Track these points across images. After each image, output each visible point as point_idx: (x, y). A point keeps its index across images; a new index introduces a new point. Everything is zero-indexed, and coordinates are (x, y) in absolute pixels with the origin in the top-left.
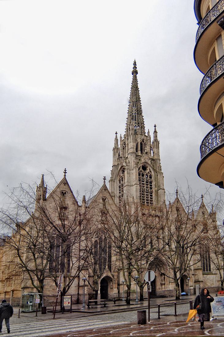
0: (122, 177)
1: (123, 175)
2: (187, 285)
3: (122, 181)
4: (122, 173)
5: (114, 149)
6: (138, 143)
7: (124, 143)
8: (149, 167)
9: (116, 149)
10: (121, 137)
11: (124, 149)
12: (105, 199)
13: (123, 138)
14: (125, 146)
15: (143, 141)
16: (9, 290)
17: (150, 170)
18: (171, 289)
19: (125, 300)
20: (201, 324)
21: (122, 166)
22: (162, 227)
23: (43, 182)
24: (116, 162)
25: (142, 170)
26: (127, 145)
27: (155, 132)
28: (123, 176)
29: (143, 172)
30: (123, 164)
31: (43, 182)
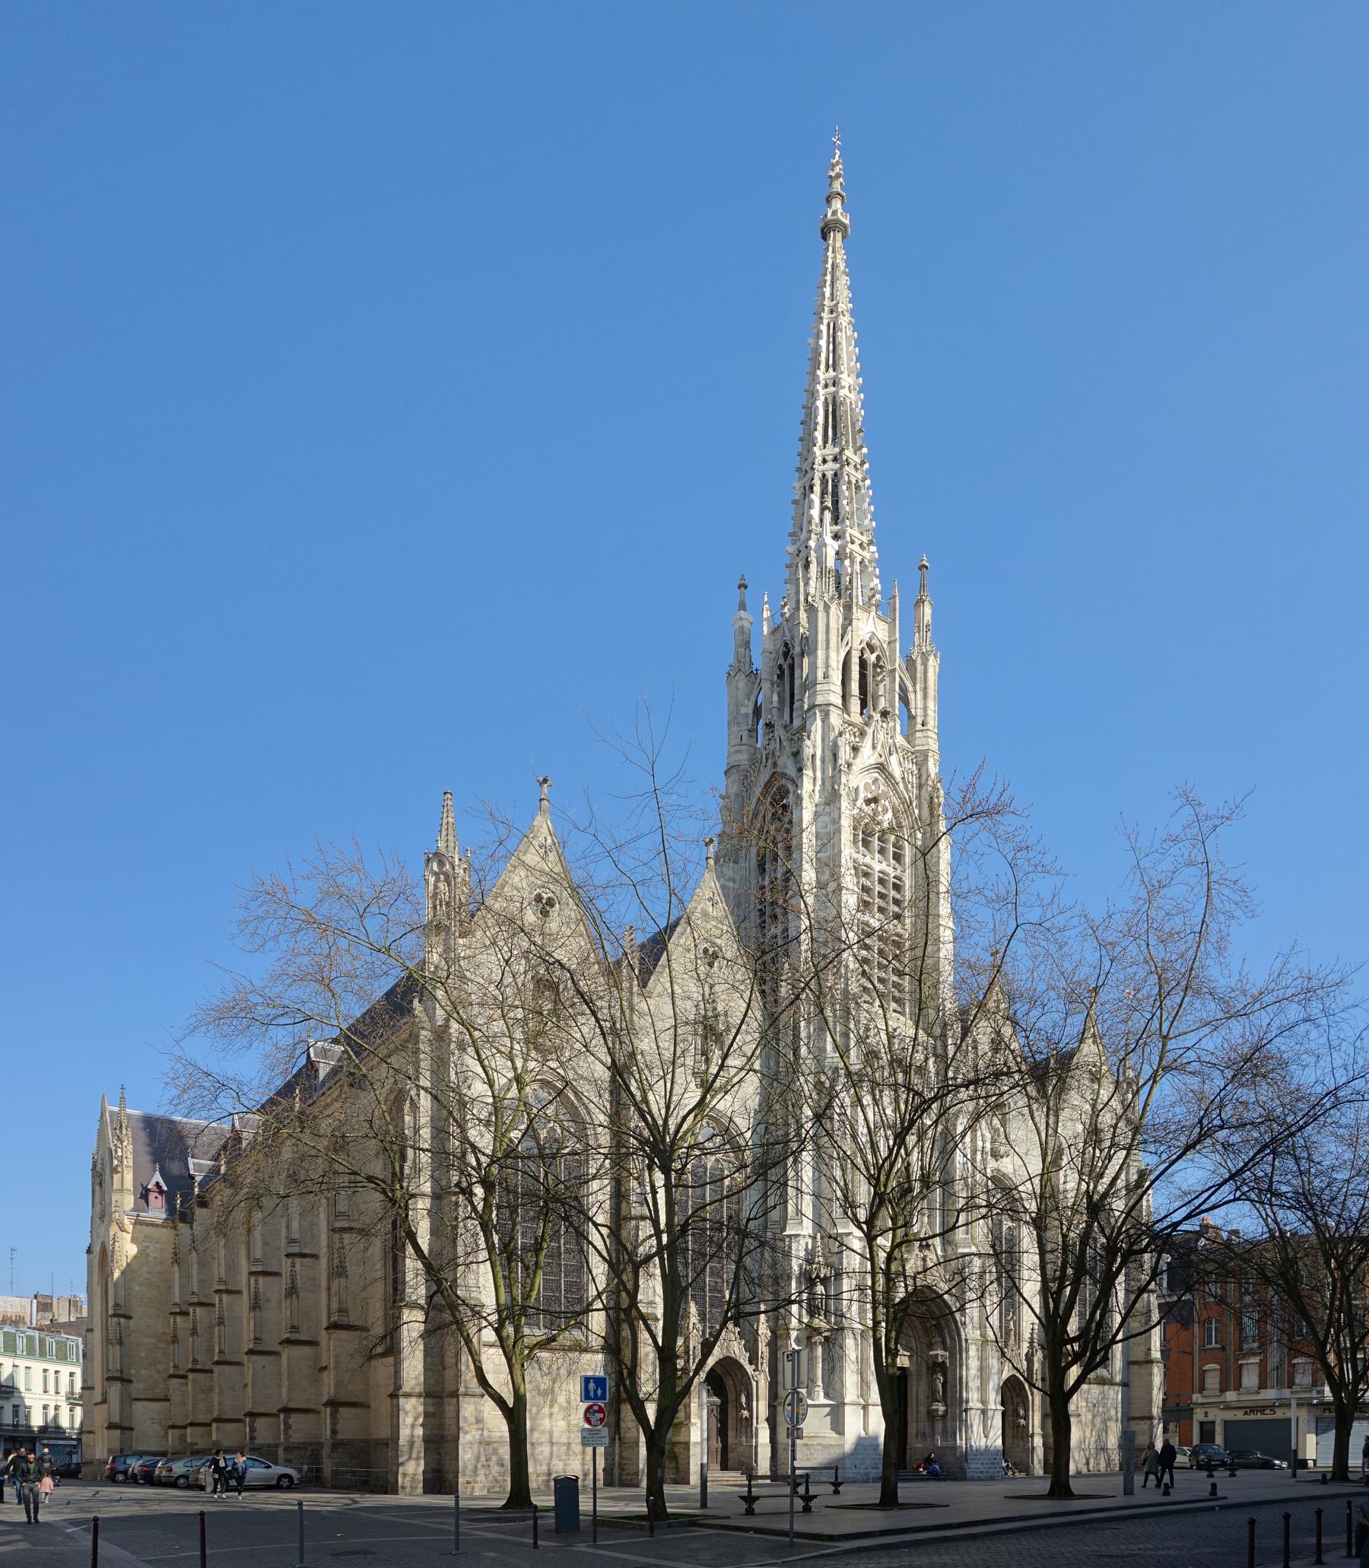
2: (121, 1343)
6: (848, 654)
7: (782, 649)
11: (781, 676)
14: (785, 667)
24: (744, 748)
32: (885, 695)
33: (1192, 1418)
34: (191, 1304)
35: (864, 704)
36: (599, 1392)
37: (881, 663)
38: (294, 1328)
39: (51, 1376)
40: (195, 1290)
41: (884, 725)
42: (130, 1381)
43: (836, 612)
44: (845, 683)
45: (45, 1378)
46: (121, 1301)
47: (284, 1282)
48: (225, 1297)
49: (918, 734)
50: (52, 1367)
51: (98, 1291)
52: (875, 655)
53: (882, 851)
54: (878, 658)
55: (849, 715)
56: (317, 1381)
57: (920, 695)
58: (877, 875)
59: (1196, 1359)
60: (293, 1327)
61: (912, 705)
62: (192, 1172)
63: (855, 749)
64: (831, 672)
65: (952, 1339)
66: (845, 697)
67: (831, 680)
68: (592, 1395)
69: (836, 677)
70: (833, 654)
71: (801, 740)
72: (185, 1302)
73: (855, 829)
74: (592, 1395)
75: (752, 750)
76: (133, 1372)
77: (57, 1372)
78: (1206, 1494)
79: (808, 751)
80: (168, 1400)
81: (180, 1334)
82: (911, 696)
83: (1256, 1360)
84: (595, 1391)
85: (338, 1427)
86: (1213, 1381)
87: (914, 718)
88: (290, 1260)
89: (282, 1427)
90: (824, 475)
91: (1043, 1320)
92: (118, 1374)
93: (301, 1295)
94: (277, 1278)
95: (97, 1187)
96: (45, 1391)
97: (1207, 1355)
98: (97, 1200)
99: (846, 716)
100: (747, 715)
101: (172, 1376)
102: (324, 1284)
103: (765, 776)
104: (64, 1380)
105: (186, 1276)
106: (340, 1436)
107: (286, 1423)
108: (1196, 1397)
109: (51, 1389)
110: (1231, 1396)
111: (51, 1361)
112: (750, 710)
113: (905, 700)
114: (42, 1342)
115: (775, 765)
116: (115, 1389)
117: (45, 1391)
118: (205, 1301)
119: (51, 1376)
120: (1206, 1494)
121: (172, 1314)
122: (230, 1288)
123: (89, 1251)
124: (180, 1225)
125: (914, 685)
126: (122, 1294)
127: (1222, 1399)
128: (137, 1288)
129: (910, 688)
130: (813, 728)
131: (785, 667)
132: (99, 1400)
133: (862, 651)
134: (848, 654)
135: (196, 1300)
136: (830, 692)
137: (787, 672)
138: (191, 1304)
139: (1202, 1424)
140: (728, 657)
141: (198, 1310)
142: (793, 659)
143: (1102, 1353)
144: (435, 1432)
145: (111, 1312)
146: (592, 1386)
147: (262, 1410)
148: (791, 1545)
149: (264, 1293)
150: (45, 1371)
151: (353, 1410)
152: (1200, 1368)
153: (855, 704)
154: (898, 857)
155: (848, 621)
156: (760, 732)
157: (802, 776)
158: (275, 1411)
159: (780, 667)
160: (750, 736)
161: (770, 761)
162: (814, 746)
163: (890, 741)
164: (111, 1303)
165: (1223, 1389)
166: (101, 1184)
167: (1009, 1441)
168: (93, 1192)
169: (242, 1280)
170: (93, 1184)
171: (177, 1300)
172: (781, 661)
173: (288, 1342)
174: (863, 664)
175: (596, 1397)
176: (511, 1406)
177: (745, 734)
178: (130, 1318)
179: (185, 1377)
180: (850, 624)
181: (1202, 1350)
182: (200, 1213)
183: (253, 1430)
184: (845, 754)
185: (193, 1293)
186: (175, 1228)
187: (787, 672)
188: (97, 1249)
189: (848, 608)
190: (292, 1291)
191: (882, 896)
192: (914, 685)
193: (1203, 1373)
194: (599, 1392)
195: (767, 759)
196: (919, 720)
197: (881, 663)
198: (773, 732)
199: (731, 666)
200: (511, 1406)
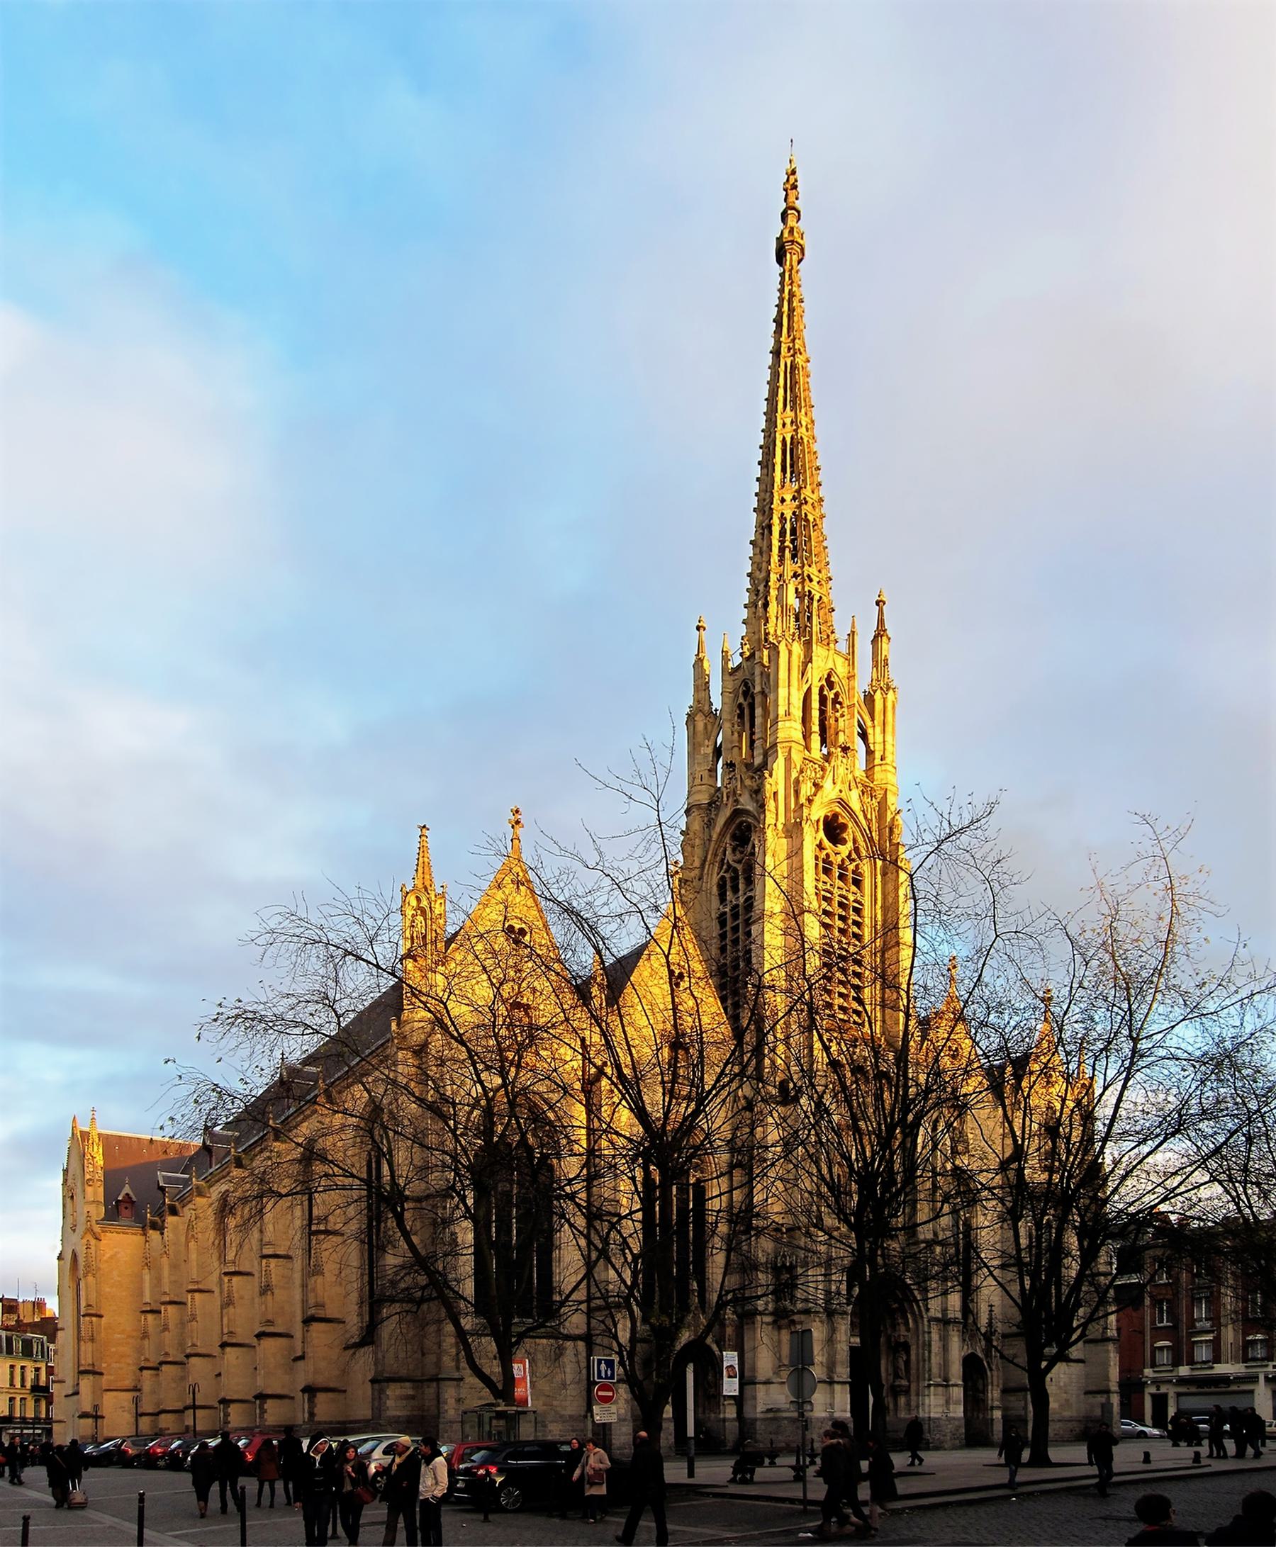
0: (735, 870)
1: (739, 862)
3: (735, 890)
4: (734, 850)
5: (691, 718)
6: (809, 689)
7: (743, 688)
8: (850, 831)
9: (700, 713)
10: (725, 659)
11: (741, 716)
12: (681, 976)
13: (736, 661)
15: (831, 685)
16: (56, 1415)
17: (855, 841)
18: (932, 1415)
19: (792, 1467)
20: (637, 1524)
21: (737, 813)
22: (744, 1108)
23: (423, 866)
25: (826, 843)
26: (758, 699)
27: (880, 633)
28: (739, 867)
29: (829, 851)
30: (741, 799)
31: (423, 866)
32: (846, 729)
33: (1143, 1392)
34: (163, 1303)
35: (823, 741)
36: (609, 1373)
37: (840, 699)
38: (270, 1322)
39: (18, 1371)
40: (167, 1290)
41: (844, 760)
42: (101, 1374)
43: (797, 649)
44: (805, 720)
45: (12, 1374)
46: (93, 1302)
47: (257, 1284)
48: (197, 1295)
49: (877, 769)
50: (19, 1364)
51: (70, 1294)
52: (834, 691)
53: (841, 877)
54: (837, 695)
55: (809, 751)
56: (291, 1369)
57: (878, 729)
58: (837, 899)
59: (1148, 1338)
60: (269, 1321)
61: (871, 739)
62: (161, 1184)
63: (817, 786)
64: (792, 710)
65: (915, 1321)
66: (806, 736)
67: (792, 717)
68: (603, 1375)
69: (797, 713)
70: (794, 690)
71: (762, 777)
72: (156, 1301)
73: (817, 858)
74: (603, 1375)
75: (713, 791)
76: (104, 1365)
77: (23, 1368)
78: (1189, 1463)
79: (769, 790)
80: (139, 1390)
81: (151, 1330)
82: (870, 731)
83: (1210, 1337)
84: (606, 1371)
85: (316, 1411)
86: (1164, 1358)
87: (873, 752)
88: (264, 1261)
89: (258, 1411)
90: (782, 514)
91: (1019, 1301)
92: (90, 1368)
93: (276, 1291)
94: (249, 1278)
95: (68, 1200)
96: (12, 1384)
97: (1158, 1333)
98: (69, 1210)
99: (806, 752)
100: (706, 755)
101: (142, 1369)
102: (298, 1281)
103: (726, 813)
104: (30, 1376)
105: (158, 1280)
106: (316, 1419)
107: (261, 1407)
108: (1148, 1372)
109: (18, 1385)
110: (1184, 1371)
111: (17, 1358)
112: (710, 750)
113: (864, 735)
114: (9, 1340)
115: (737, 801)
116: (86, 1383)
117: (12, 1384)
118: (176, 1299)
119: (18, 1371)
120: (1189, 1463)
121: (143, 1312)
122: (201, 1287)
123: (60, 1258)
124: (151, 1232)
125: (873, 720)
126: (93, 1296)
127: (1174, 1374)
128: (108, 1290)
129: (869, 723)
130: (775, 766)
131: (745, 704)
132: (70, 1392)
133: (821, 689)
134: (809, 689)
135: (168, 1299)
136: (790, 729)
137: (747, 712)
138: (163, 1303)
139: (1153, 1395)
140: (687, 700)
141: (170, 1308)
142: (753, 699)
143: (1079, 1331)
144: (415, 1413)
145: (225, 1331)
146: (603, 1366)
147: (235, 1397)
148: (805, 1512)
149: (237, 1292)
150: (12, 1367)
151: (330, 1395)
152: (1152, 1345)
153: (816, 739)
154: (857, 883)
155: (808, 659)
156: (720, 771)
157: (764, 812)
158: (250, 1398)
159: (740, 706)
160: (710, 776)
161: (731, 799)
162: (777, 783)
163: (850, 777)
164: (83, 1304)
165: (1176, 1363)
166: (72, 1197)
167: (969, 1414)
168: (64, 1206)
169: (212, 1282)
170: (64, 1196)
171: (148, 1300)
172: (741, 700)
173: (260, 1336)
174: (823, 700)
175: (607, 1378)
176: (217, 1483)
177: (706, 774)
178: (100, 1316)
179: (156, 1369)
180: (811, 661)
181: (1154, 1329)
182: (170, 1220)
183: (227, 1415)
184: (807, 789)
185: (165, 1293)
186: (145, 1234)
187: (747, 712)
188: (68, 1256)
189: (808, 645)
190: (266, 1289)
191: (842, 918)
192: (873, 720)
193: (1154, 1350)
194: (609, 1373)
195: (728, 797)
196: (878, 755)
197: (840, 699)
198: (734, 770)
199: (691, 707)
200: (217, 1483)
